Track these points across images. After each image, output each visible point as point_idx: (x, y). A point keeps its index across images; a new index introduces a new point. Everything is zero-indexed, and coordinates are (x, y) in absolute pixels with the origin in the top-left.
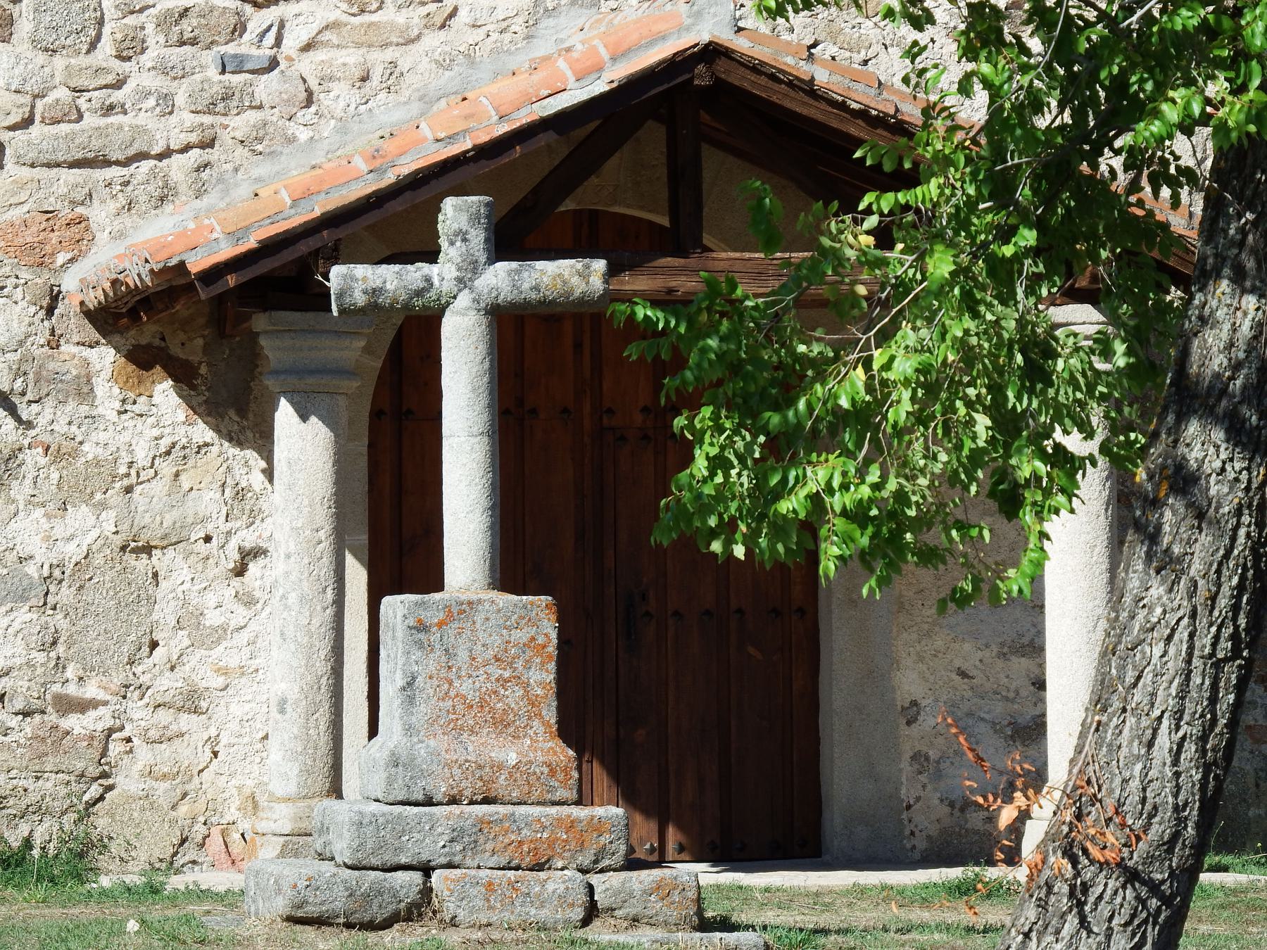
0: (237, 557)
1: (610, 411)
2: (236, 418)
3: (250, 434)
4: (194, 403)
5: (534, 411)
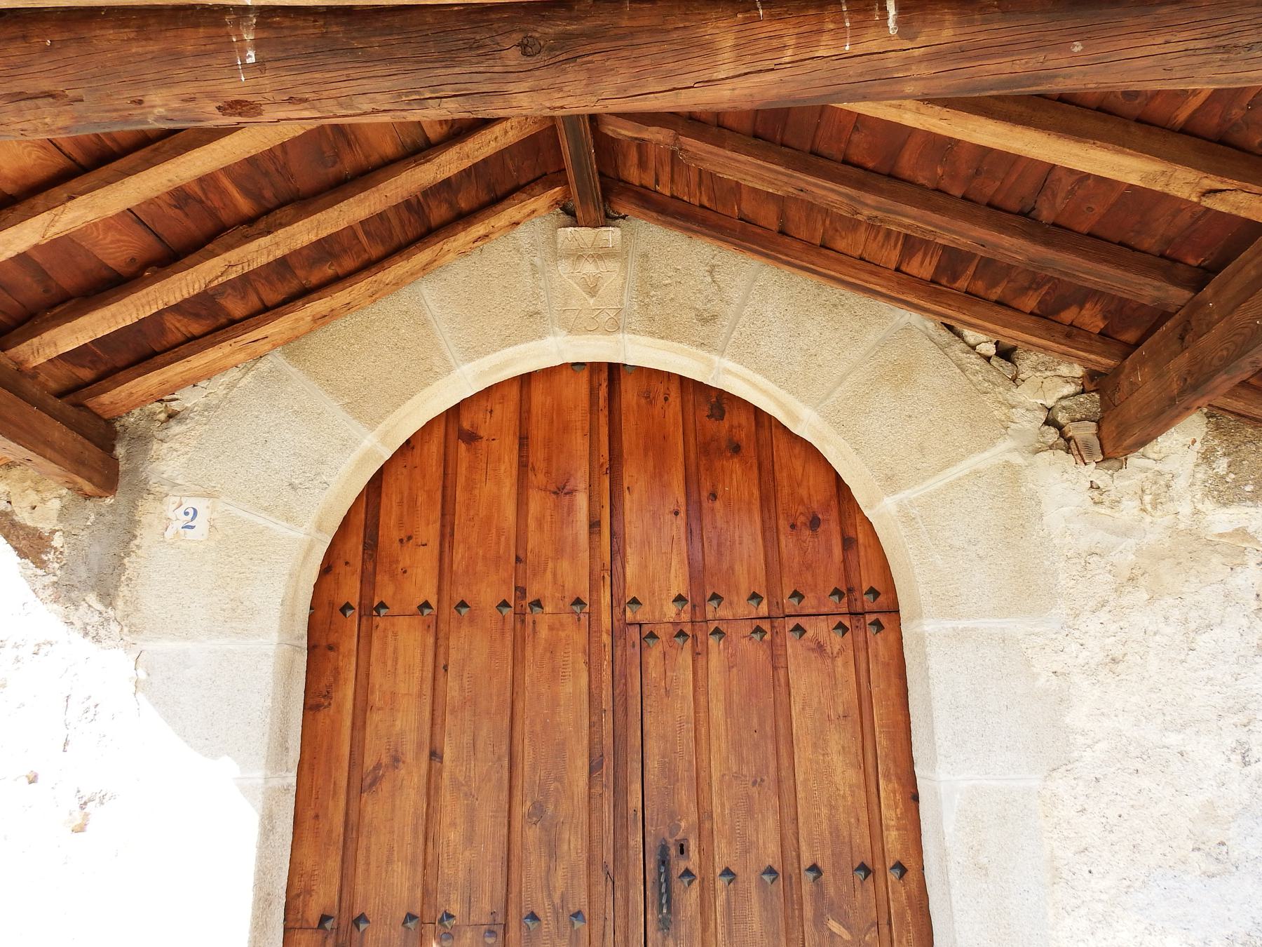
0: (75, 805)
1: (635, 601)
2: (100, 607)
3: (114, 627)
4: (38, 586)
5: (538, 603)
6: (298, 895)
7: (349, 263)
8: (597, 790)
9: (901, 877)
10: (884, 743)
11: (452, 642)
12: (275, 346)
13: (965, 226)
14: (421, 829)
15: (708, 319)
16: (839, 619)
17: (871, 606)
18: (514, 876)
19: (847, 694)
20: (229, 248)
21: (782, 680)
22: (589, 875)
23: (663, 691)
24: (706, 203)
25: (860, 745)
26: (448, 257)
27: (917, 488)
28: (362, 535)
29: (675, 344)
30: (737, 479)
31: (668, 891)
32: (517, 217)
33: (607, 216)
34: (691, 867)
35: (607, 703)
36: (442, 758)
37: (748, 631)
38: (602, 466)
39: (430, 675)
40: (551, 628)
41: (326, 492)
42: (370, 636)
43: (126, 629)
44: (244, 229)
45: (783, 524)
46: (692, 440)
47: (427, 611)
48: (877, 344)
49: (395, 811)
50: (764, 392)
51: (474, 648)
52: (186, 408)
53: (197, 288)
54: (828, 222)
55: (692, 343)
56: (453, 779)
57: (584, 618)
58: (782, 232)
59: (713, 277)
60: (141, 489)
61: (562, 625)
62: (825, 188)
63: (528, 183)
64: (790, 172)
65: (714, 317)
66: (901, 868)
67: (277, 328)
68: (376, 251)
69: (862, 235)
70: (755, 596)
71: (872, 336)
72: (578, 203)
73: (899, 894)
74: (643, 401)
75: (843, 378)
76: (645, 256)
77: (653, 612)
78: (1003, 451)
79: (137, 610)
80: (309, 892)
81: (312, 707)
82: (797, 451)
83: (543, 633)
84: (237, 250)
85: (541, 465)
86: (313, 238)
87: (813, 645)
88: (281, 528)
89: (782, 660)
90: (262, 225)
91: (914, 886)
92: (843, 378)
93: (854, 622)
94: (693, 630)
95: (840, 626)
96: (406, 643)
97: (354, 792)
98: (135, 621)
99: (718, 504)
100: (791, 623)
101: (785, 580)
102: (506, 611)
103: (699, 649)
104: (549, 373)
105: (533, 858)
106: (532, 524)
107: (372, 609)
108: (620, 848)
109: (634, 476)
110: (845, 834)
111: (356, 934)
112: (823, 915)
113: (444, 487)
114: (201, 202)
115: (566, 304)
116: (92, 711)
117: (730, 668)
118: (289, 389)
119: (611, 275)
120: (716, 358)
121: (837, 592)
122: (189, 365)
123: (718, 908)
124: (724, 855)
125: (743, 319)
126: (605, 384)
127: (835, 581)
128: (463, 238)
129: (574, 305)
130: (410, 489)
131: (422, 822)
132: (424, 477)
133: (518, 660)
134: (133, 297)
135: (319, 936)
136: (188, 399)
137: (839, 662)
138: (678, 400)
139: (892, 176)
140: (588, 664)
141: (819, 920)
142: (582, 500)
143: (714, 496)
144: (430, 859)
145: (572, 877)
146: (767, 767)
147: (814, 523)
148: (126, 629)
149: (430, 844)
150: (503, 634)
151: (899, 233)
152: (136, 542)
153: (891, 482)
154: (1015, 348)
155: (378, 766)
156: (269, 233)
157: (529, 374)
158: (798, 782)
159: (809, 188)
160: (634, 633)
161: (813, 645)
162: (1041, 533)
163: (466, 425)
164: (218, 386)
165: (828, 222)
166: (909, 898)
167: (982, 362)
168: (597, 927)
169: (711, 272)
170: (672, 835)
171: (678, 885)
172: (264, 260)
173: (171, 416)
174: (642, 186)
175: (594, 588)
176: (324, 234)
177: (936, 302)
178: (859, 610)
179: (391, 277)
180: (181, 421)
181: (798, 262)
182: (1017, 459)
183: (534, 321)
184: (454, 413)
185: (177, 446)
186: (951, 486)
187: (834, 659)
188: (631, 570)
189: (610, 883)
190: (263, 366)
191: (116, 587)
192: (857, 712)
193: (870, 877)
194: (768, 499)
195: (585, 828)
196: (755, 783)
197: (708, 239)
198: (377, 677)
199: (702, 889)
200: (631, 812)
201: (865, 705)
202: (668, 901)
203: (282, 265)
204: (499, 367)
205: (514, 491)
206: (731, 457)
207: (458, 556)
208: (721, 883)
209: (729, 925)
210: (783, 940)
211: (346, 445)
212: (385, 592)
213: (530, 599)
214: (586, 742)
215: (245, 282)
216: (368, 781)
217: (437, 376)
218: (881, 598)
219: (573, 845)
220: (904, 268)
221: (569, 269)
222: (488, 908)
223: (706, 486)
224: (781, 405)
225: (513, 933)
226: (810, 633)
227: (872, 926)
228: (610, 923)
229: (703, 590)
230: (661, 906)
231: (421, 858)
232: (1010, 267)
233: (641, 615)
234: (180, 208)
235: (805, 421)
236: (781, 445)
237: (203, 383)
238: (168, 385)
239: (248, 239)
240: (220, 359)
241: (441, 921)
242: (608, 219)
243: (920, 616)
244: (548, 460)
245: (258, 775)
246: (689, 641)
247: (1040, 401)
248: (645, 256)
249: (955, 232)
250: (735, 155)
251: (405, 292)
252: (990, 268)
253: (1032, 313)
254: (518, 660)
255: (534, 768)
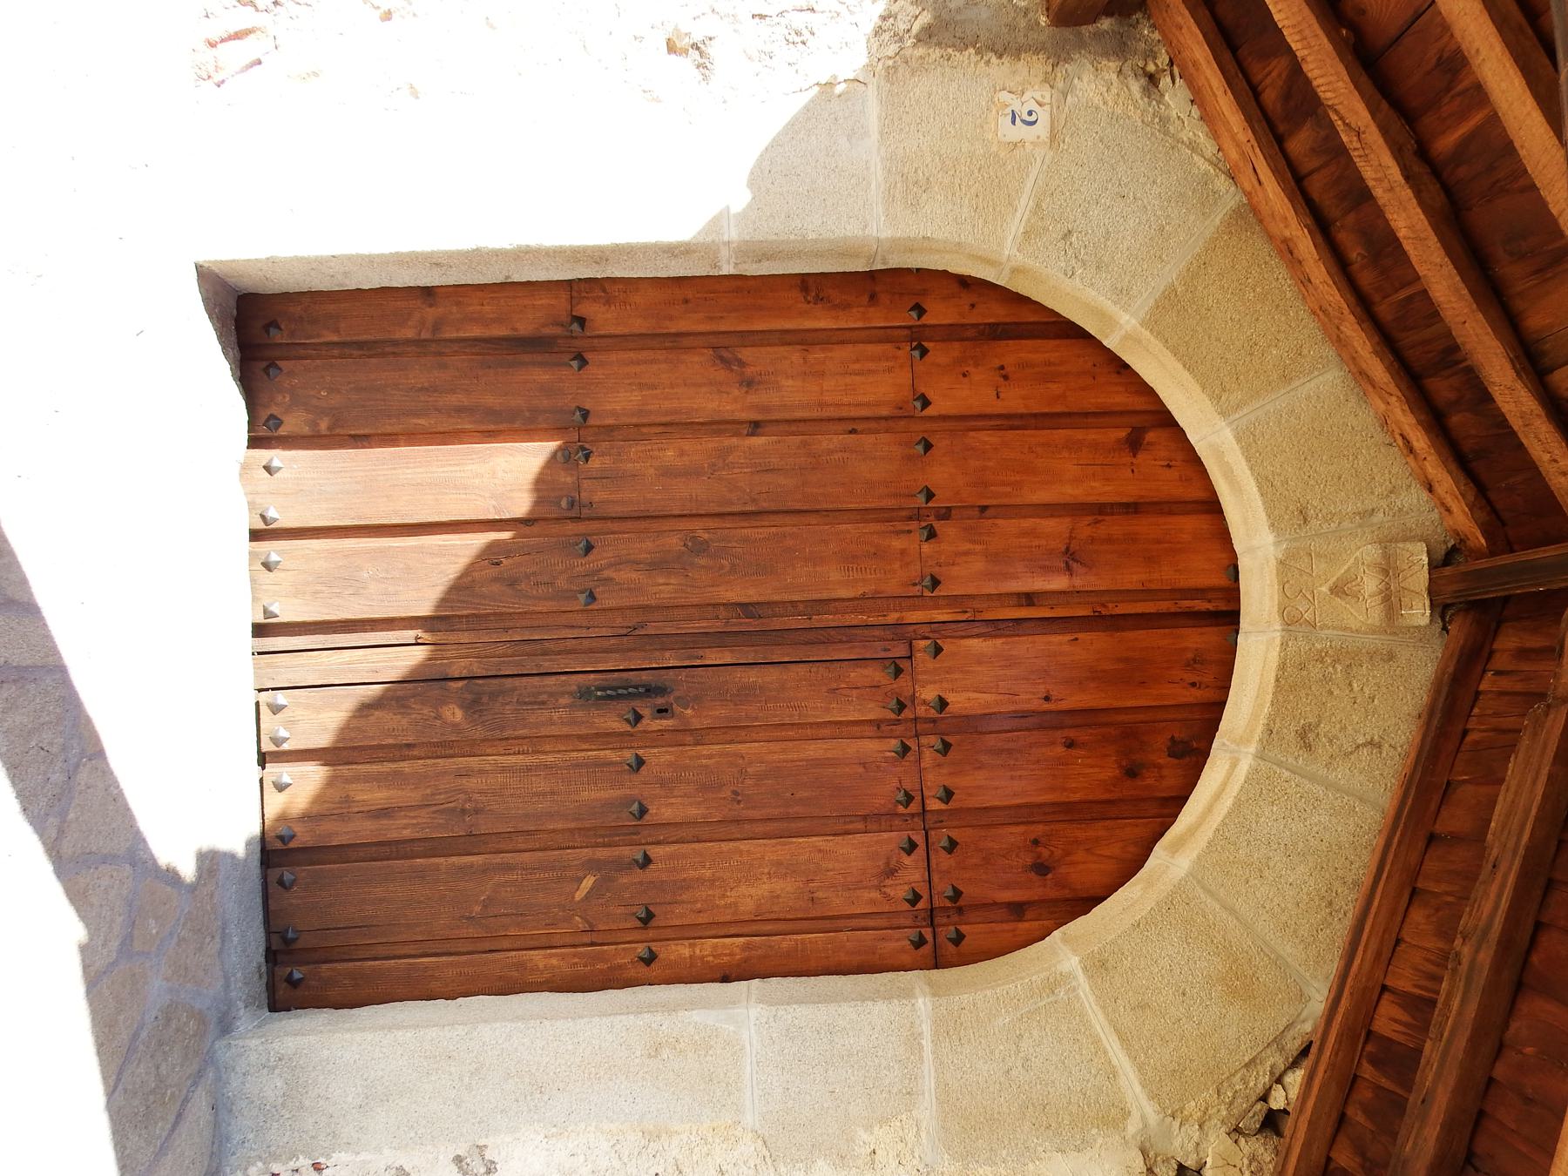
0: (697, 37)
1: (938, 650)
2: (916, 28)
3: (892, 49)
5: (932, 535)
6: (604, 291)
7: (1366, 279)
8: (722, 612)
9: (642, 959)
10: (785, 945)
11: (883, 437)
12: (1248, 194)
13: (1451, 1078)
14: (676, 418)
15: (1305, 738)
16: (926, 897)
17: (945, 931)
18: (629, 525)
19: (838, 903)
20: (1384, 131)
21: (851, 827)
22: (631, 608)
23: (834, 686)
24: (1468, 739)
25: (782, 916)
26: (1379, 402)
27: (1092, 998)
28: (1008, 320)
29: (1269, 697)
30: (1092, 774)
31: (619, 697)
32: (1440, 490)
33: (1446, 607)
34: (644, 721)
35: (816, 621)
36: (753, 435)
37: (908, 786)
38: (1104, 606)
39: (844, 414)
40: (903, 552)
41: (1062, 276)
42: (888, 340)
43: (890, 63)
44: (1411, 145)
45: (1039, 830)
46: (1141, 717)
47: (918, 405)
48: (1279, 957)
49: (699, 391)
50: (1209, 809)
51: (876, 463)
52: (1162, 95)
53: (1326, 95)
54: (1450, 899)
55: (1271, 719)
56: (730, 450)
57: (916, 590)
58: (1432, 839)
59: (1364, 745)
60: (1059, 55)
61: (908, 564)
62: (1499, 896)
63: (1489, 502)
64: (1521, 851)
65: (1308, 747)
66: (649, 960)
67: (1274, 195)
68: (1385, 310)
69: (1433, 944)
70: (948, 795)
71: (1289, 950)
72: (1463, 568)
73: (625, 955)
74: (1190, 655)
75: (1232, 911)
76: (1391, 657)
77: (925, 672)
78: (1143, 1110)
79: (913, 73)
80: (608, 302)
81: (812, 287)
82: (1132, 849)
83: (897, 543)
84: (1381, 141)
85: (1102, 531)
86: (1401, 234)
87: (893, 862)
88: (1015, 226)
89: (875, 827)
90: (1418, 168)
91: (632, 973)
92: (1232, 911)
93: (923, 914)
94: (906, 720)
95: (915, 898)
96: (879, 383)
97: (713, 340)
98: (901, 70)
99: (1060, 750)
100: (918, 838)
101: (969, 831)
102: (922, 498)
103: (883, 727)
104: (1223, 536)
105: (649, 545)
106: (1027, 523)
107: (919, 340)
108: (662, 641)
109: (1095, 646)
110: (684, 897)
111: (566, 358)
112: (599, 870)
113: (1069, 414)
114: (1449, 89)
115: (1319, 555)
116: (798, 38)
117: (864, 765)
118: (1192, 218)
119: (1364, 613)
120: (1252, 748)
121: (958, 893)
122: (1220, 93)
123: (602, 753)
124: (658, 758)
125: (1308, 785)
126: (1210, 607)
127: (969, 891)
128: (1407, 421)
129: (1320, 567)
130: (1067, 373)
131: (684, 418)
132: (1083, 389)
133: (865, 515)
134: (1313, 20)
135: (565, 318)
136: (1175, 97)
137: (875, 895)
138: (1191, 700)
139: (1519, 987)
140: (863, 597)
141: (592, 866)
142: (1059, 583)
143: (1070, 744)
144: (644, 430)
145: (629, 589)
146: (754, 808)
147: (1041, 869)
148: (890, 63)
149: (660, 430)
150: (895, 495)
151: (1438, 993)
152: (994, 59)
153: (1098, 966)
154: (1279, 1134)
155: (742, 364)
156: (1407, 178)
157: (1221, 512)
158: (737, 844)
159: (1499, 876)
160: (900, 650)
161: (893, 862)
162: (1040, 1149)
163: (1151, 436)
164: (1192, 129)
165: (1450, 899)
166: (620, 967)
167: (1260, 1090)
168: (579, 619)
169: (1371, 743)
170: (677, 699)
171: (624, 707)
172: (1368, 173)
173: (1152, 79)
174: (1492, 653)
175: (954, 601)
176: (1408, 246)
177: (1340, 1036)
178: (937, 920)
179: (1349, 333)
180: (1146, 92)
181: (1391, 857)
182: (1133, 1126)
183: (1293, 516)
184: (1166, 421)
185: (1114, 91)
186: (1097, 1041)
187: (878, 888)
188: (975, 644)
189: (624, 631)
190: (1222, 183)
191: (939, 44)
192: (819, 914)
193: (639, 924)
194: (1070, 812)
195: (682, 601)
196: (735, 793)
197: (1418, 740)
198: (841, 353)
199: (621, 734)
200: (701, 652)
201: (827, 924)
202: (609, 697)
203: (1361, 195)
204: (1229, 474)
205: (1069, 500)
206: (1121, 767)
207: (984, 436)
208: (629, 755)
209: (586, 765)
210: (573, 825)
211: (1121, 294)
212: (940, 354)
213: (937, 525)
214: (776, 598)
215: (1335, 151)
216: (725, 354)
217: (1216, 398)
218: (951, 948)
219: (664, 588)
220: (1386, 996)
221: (1368, 559)
222: (596, 498)
223: (1081, 735)
224: (1192, 831)
225: (571, 527)
226: (907, 860)
227: (590, 925)
228: (584, 633)
229: (952, 731)
230: (603, 689)
231: (645, 421)
232: (1394, 1135)
233: (922, 657)
234: (1438, 64)
235: (1172, 860)
236: (1134, 830)
237: (1196, 112)
238: (1192, 70)
239: (1397, 152)
240: (1230, 130)
241: (583, 448)
242: (1442, 608)
243: (934, 995)
244: (1109, 540)
245: (733, 234)
246: (893, 716)
247: (1209, 1160)
248: (1391, 657)
249: (1441, 1065)
250: (1543, 778)
251: (1329, 352)
252: (1391, 1111)
253: (1329, 1159)
254: (865, 515)
255: (746, 540)
